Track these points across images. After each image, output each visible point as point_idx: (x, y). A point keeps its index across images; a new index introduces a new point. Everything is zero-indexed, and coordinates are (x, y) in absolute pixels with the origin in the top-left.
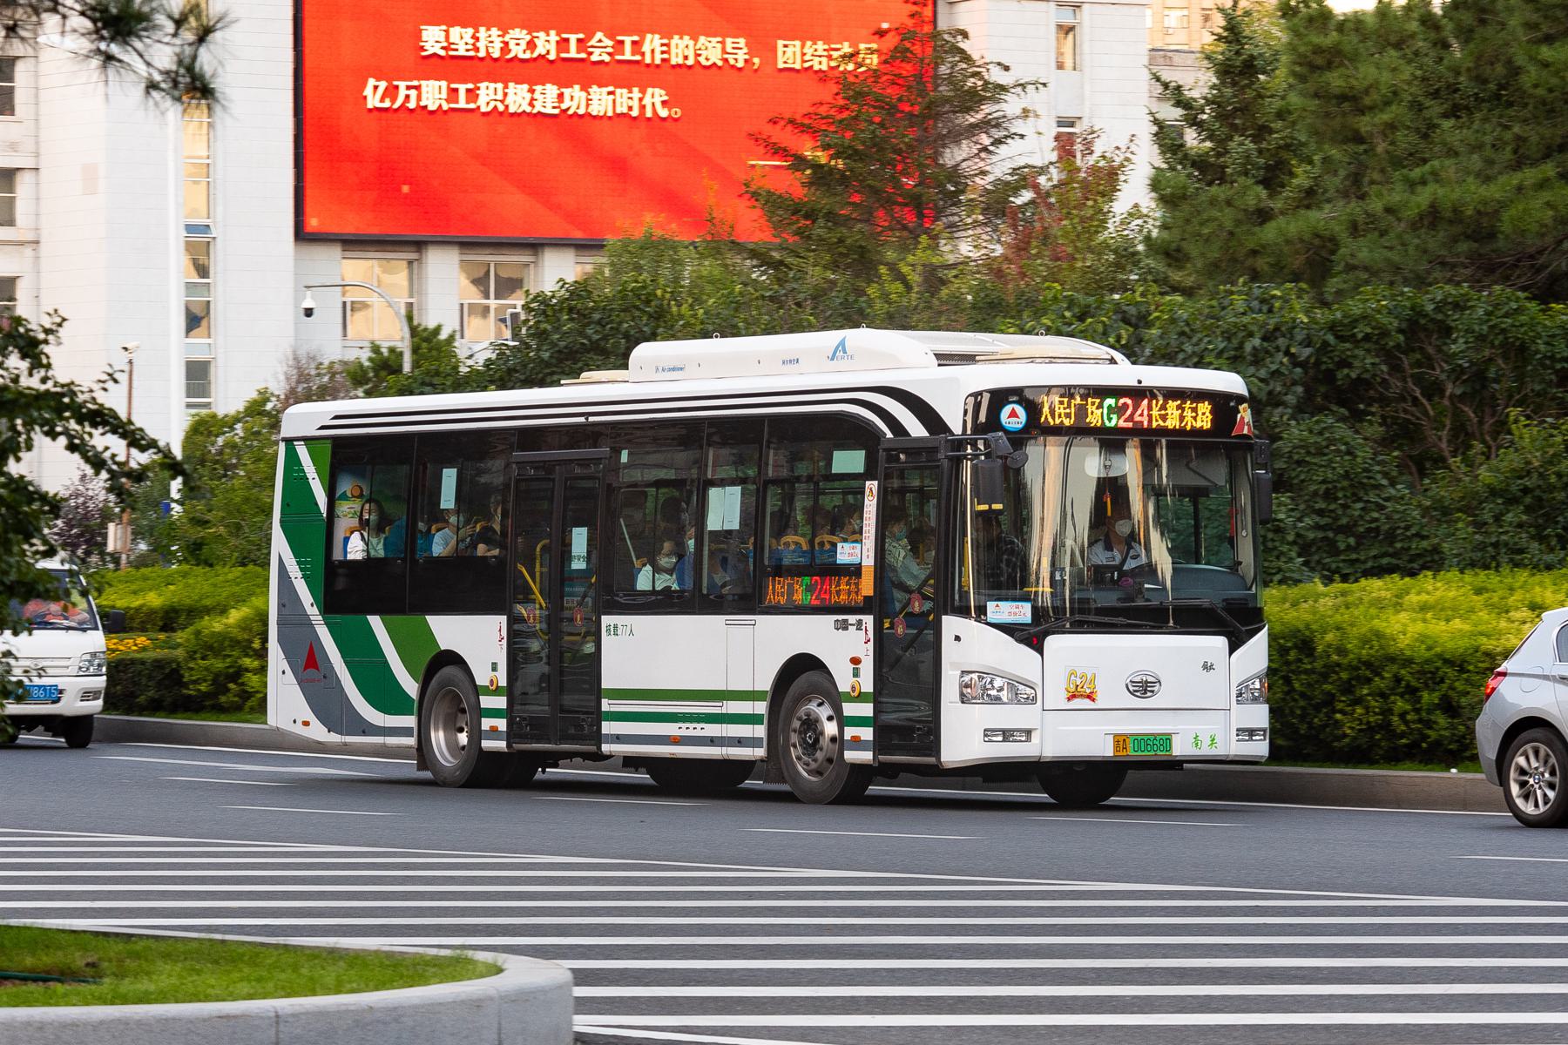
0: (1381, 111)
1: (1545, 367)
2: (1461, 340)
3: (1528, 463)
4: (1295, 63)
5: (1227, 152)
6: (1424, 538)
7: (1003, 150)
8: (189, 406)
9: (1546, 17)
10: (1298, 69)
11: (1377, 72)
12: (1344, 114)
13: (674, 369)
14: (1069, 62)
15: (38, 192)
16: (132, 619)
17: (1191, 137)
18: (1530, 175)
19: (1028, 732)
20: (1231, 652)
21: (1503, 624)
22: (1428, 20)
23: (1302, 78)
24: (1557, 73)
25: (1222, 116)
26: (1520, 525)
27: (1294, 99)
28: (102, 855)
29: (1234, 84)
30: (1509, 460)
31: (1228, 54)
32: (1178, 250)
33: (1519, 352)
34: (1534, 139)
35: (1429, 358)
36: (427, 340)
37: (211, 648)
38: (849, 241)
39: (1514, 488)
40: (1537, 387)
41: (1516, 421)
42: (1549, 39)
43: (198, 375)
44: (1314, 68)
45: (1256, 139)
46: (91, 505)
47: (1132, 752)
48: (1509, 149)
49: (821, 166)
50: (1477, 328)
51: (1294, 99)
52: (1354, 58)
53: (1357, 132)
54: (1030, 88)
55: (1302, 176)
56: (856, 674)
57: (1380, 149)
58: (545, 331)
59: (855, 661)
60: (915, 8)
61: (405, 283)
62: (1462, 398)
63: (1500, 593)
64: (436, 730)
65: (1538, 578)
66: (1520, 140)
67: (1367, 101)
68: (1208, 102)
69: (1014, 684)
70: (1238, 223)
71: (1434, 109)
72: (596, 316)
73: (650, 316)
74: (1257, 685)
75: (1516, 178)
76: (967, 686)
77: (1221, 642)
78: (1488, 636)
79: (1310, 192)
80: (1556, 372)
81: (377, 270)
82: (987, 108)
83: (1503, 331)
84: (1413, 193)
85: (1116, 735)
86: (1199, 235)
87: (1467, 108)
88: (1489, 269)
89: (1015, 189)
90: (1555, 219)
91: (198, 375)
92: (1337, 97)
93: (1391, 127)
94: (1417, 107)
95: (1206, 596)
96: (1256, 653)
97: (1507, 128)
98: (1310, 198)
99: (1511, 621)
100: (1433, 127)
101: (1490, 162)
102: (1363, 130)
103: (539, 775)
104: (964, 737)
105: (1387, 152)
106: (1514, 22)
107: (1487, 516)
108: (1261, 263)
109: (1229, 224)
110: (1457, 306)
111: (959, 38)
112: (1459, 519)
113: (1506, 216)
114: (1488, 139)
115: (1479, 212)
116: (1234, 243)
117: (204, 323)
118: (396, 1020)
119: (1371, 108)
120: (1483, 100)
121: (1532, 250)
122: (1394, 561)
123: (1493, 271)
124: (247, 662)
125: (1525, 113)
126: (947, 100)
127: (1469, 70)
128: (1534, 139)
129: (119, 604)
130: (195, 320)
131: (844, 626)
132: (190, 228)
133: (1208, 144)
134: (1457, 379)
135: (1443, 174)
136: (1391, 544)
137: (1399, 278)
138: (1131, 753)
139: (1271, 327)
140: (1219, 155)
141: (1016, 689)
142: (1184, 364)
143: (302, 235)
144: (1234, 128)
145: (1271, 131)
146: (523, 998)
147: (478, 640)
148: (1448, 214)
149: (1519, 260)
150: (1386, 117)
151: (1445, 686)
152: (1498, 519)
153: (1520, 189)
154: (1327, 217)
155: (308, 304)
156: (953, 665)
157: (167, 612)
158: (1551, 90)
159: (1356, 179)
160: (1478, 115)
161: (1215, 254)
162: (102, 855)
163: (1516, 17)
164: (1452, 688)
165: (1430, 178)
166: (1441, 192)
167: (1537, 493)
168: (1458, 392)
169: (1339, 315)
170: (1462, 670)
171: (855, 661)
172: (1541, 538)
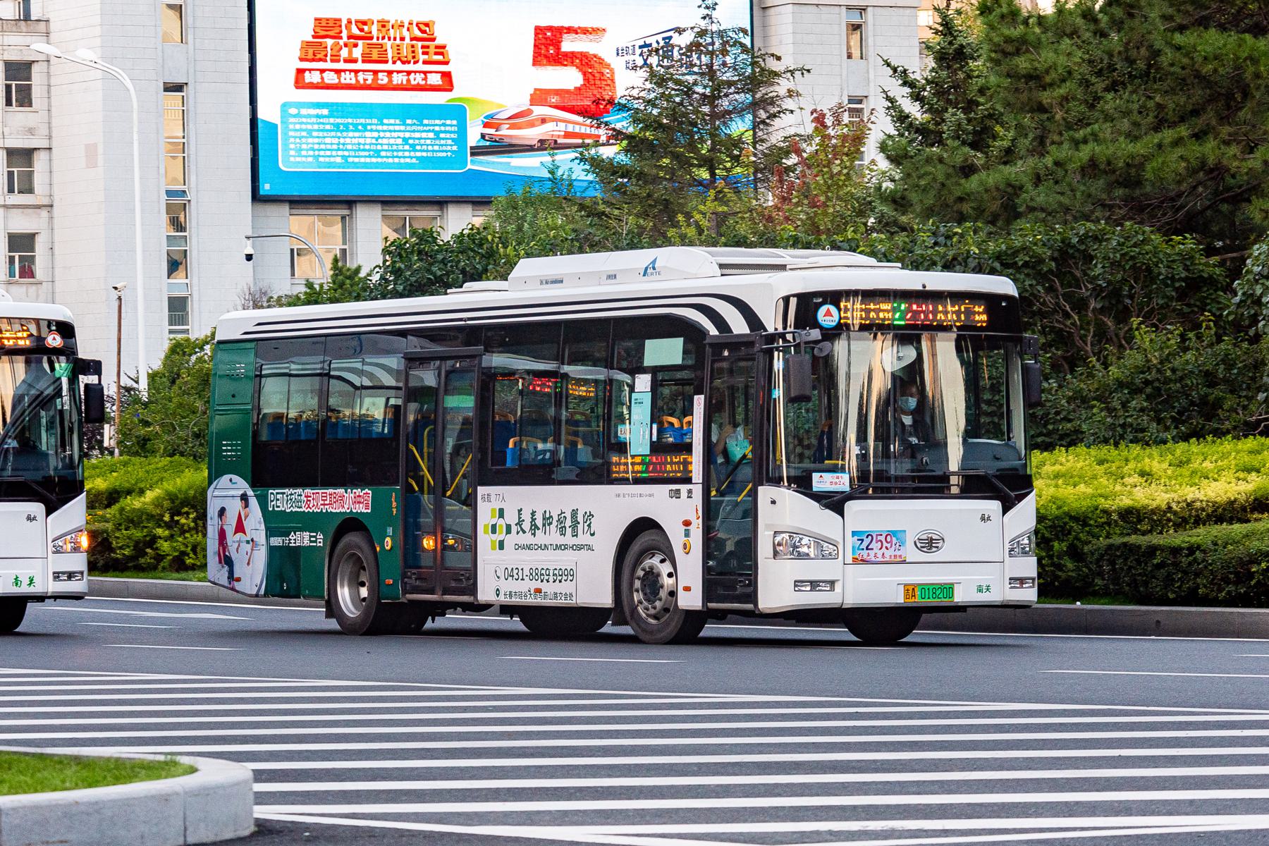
0: (1059, 87)
1: (1167, 286)
2: (1100, 266)
3: (1148, 361)
4: (991, 51)
5: (943, 121)
6: (1070, 421)
7: (777, 123)
8: (171, 332)
9: (1179, 11)
10: (993, 55)
11: (1057, 56)
13: (553, 282)
14: (856, 53)
17: (914, 110)
18: (1168, 135)
19: (832, 583)
20: (1004, 513)
21: (1118, 488)
22: (1088, 15)
23: (997, 62)
24: (1187, 55)
25: (940, 93)
26: (1142, 410)
27: (993, 79)
28: (536, 708)
29: (949, 67)
30: (1133, 358)
32: (903, 198)
33: (1145, 274)
34: (1171, 106)
35: (1077, 280)
36: (349, 278)
37: (132, 521)
39: (1137, 381)
40: (1161, 302)
41: (1137, 329)
42: (1182, 29)
43: (178, 308)
44: (1006, 54)
45: (966, 110)
47: (919, 600)
48: (1151, 114)
51: (993, 79)
52: (1038, 45)
53: (1040, 103)
54: (798, 74)
55: (1004, 136)
56: (687, 534)
57: (1058, 117)
58: (400, 269)
59: (687, 523)
60: (707, 12)
61: (340, 233)
62: (1102, 310)
63: (1117, 463)
64: (342, 586)
65: (1148, 451)
66: (1160, 106)
67: (1048, 79)
69: (819, 541)
70: (948, 176)
71: (1099, 85)
72: (440, 257)
73: (483, 256)
74: (1026, 541)
76: (779, 544)
77: (995, 505)
78: (1106, 498)
79: (1009, 151)
80: (1176, 289)
81: (318, 225)
82: (763, 90)
83: (1132, 258)
84: (1077, 150)
85: (905, 585)
86: (917, 186)
87: (1123, 83)
88: (1139, 209)
89: (787, 154)
90: (1187, 168)
91: (178, 308)
92: (1024, 76)
93: (1065, 99)
94: (1085, 83)
95: (986, 467)
96: (1024, 516)
97: (1150, 98)
98: (1009, 155)
100: (1097, 99)
101: (1136, 124)
102: (1044, 102)
103: (429, 624)
104: (778, 587)
105: (1064, 119)
106: (1154, 15)
107: (1116, 404)
108: (966, 208)
109: (941, 178)
110: (1096, 239)
111: (741, 35)
112: (1093, 406)
113: (1148, 167)
114: (1135, 106)
115: (1128, 164)
116: (945, 192)
117: (181, 268)
118: (98, 812)
119: (1051, 85)
120: (1136, 77)
121: (1172, 194)
122: (1047, 440)
124: (159, 531)
126: (730, 84)
127: (1120, 53)
128: (1171, 106)
130: (175, 265)
131: (677, 494)
132: (169, 193)
135: (1101, 135)
136: (1045, 426)
137: (1069, 218)
138: (919, 599)
139: (950, 258)
140: (937, 124)
141: (815, 547)
143: (256, 197)
144: (949, 102)
145: (978, 104)
146: (206, 793)
148: (1102, 167)
149: (1162, 202)
150: (1062, 91)
151: (1071, 537)
152: (1124, 405)
153: (1160, 146)
154: (1019, 170)
155: (250, 251)
156: (768, 527)
157: (111, 494)
158: (1183, 68)
159: (1041, 140)
160: (1130, 88)
161: (930, 201)
162: (536, 708)
163: (1155, 11)
164: (1077, 538)
165: (1091, 138)
167: (1156, 384)
168: (1099, 306)
169: (1004, 247)
170: (1085, 524)
171: (687, 523)
172: (1159, 421)
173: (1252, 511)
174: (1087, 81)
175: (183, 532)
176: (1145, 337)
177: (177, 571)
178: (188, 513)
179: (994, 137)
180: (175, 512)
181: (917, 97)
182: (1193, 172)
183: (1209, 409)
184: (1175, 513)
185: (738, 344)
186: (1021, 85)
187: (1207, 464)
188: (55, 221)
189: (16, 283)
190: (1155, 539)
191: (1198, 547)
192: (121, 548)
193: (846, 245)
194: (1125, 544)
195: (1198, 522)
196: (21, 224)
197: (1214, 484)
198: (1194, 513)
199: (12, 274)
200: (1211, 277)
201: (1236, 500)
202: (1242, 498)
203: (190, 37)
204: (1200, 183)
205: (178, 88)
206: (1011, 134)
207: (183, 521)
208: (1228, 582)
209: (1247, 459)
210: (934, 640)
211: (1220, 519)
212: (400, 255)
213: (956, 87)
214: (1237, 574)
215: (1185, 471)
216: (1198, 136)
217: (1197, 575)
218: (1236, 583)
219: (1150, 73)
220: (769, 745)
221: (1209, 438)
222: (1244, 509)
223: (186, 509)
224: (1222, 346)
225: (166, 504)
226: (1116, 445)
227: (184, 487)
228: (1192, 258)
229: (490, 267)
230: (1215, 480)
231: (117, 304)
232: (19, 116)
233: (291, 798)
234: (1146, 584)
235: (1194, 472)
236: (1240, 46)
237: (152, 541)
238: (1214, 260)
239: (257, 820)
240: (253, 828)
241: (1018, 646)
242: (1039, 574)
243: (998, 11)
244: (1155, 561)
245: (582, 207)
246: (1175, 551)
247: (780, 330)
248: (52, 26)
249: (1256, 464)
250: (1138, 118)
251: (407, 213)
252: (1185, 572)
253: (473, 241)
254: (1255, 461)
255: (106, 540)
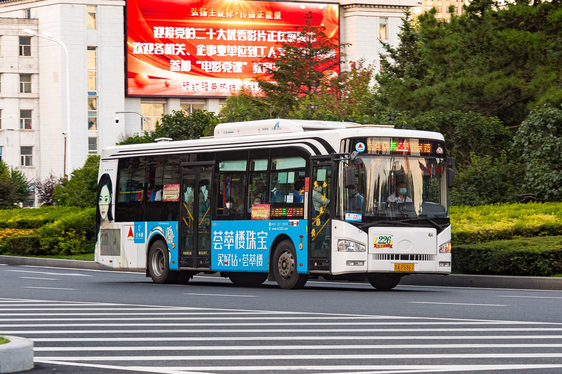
0: (452, 53)
3: (476, 170)
11: (452, 40)
12: (440, 54)
13: (230, 132)
15: (38, 82)
16: (34, 224)
17: (392, 61)
18: (495, 74)
24: (503, 40)
25: (403, 55)
26: (473, 191)
30: (471, 169)
31: (405, 34)
33: (478, 134)
34: (496, 61)
37: (49, 234)
38: (285, 97)
40: (484, 145)
41: (472, 156)
42: (501, 29)
43: (93, 142)
44: (430, 38)
45: (414, 62)
46: (54, 186)
47: (403, 270)
49: (276, 72)
50: (463, 125)
51: (424, 49)
52: (443, 35)
57: (451, 66)
63: (458, 214)
65: (472, 208)
67: (447, 49)
68: (399, 50)
69: (358, 244)
70: (404, 90)
71: (468, 52)
72: (185, 123)
75: (489, 75)
77: (433, 231)
79: (432, 80)
80: (491, 140)
91: (93, 142)
93: (454, 59)
95: (431, 215)
96: (446, 234)
97: (487, 58)
98: (432, 82)
99: (460, 223)
100: (467, 58)
101: (481, 70)
102: (446, 59)
104: (340, 264)
106: (489, 23)
107: (462, 188)
108: (412, 104)
109: (401, 91)
110: (457, 118)
115: (477, 87)
119: (449, 52)
120: (483, 49)
121: (497, 99)
123: (484, 106)
124: (60, 238)
125: (493, 53)
127: (475, 39)
129: (30, 219)
130: (91, 124)
132: (90, 93)
133: (399, 64)
134: (457, 142)
138: (400, 270)
141: (354, 247)
142: (134, 143)
143: (127, 95)
145: (419, 60)
146: (10, 352)
147: (169, 231)
149: (493, 103)
152: (466, 189)
153: (491, 79)
159: (445, 75)
166: (464, 80)
167: (479, 180)
168: (458, 147)
169: (417, 121)
172: (481, 196)
173: (514, 235)
174: (463, 50)
175: (70, 239)
176: (475, 159)
177: (67, 255)
178: (72, 231)
179: (426, 74)
180: (67, 230)
181: (393, 57)
182: (505, 90)
183: (502, 191)
184: (481, 235)
185: (324, 159)
186: (436, 52)
187: (496, 215)
188: (41, 105)
189: (24, 131)
190: (472, 246)
191: (489, 250)
192: (44, 245)
193: (352, 120)
194: (458, 248)
195: (491, 239)
196: (26, 106)
197: (498, 223)
198: (489, 235)
199: (22, 127)
200: (506, 135)
201: (507, 230)
202: (510, 229)
203: (99, 27)
204: (509, 94)
205: (93, 48)
206: (433, 73)
207: (70, 234)
208: (501, 265)
209: (513, 212)
210: (412, 289)
211: (500, 238)
212: (168, 122)
213: (410, 52)
214: (505, 261)
215: (486, 217)
216: (508, 75)
217: (488, 261)
218: (505, 265)
219: (489, 48)
220: (271, 333)
221: (499, 203)
222: (510, 234)
223: (71, 229)
224: (509, 164)
225: (63, 227)
226: (537, 203)
227: (71, 220)
228: (498, 126)
229: (206, 127)
230: (499, 221)
231: (64, 140)
232: (25, 60)
233: (545, 350)
234: (467, 265)
235: (490, 218)
236: (525, 36)
237: (57, 243)
238: (507, 128)
239: (35, 363)
240: (33, 367)
241: (435, 292)
242: (452, 260)
243: (427, 20)
244: (471, 256)
245: (254, 102)
246: (479, 251)
247: (343, 152)
248: (40, 21)
249: (517, 215)
250: (482, 67)
251: (191, 103)
252: (483, 260)
253: (199, 116)
254: (516, 213)
255: (38, 242)
